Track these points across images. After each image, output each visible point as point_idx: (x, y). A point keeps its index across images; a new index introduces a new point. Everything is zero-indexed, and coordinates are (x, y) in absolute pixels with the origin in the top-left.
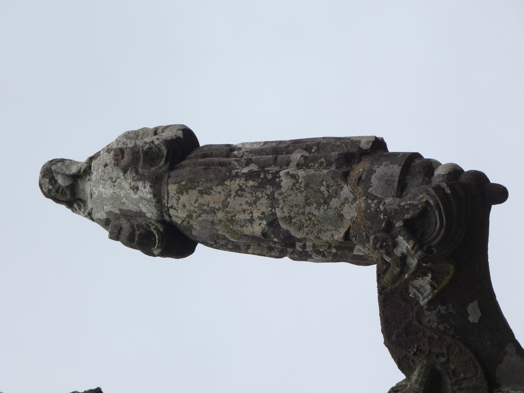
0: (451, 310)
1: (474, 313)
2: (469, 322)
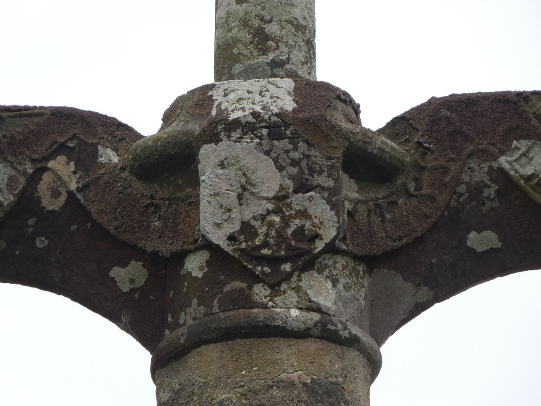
0: (488, 204)
1: (480, 240)
2: (469, 232)
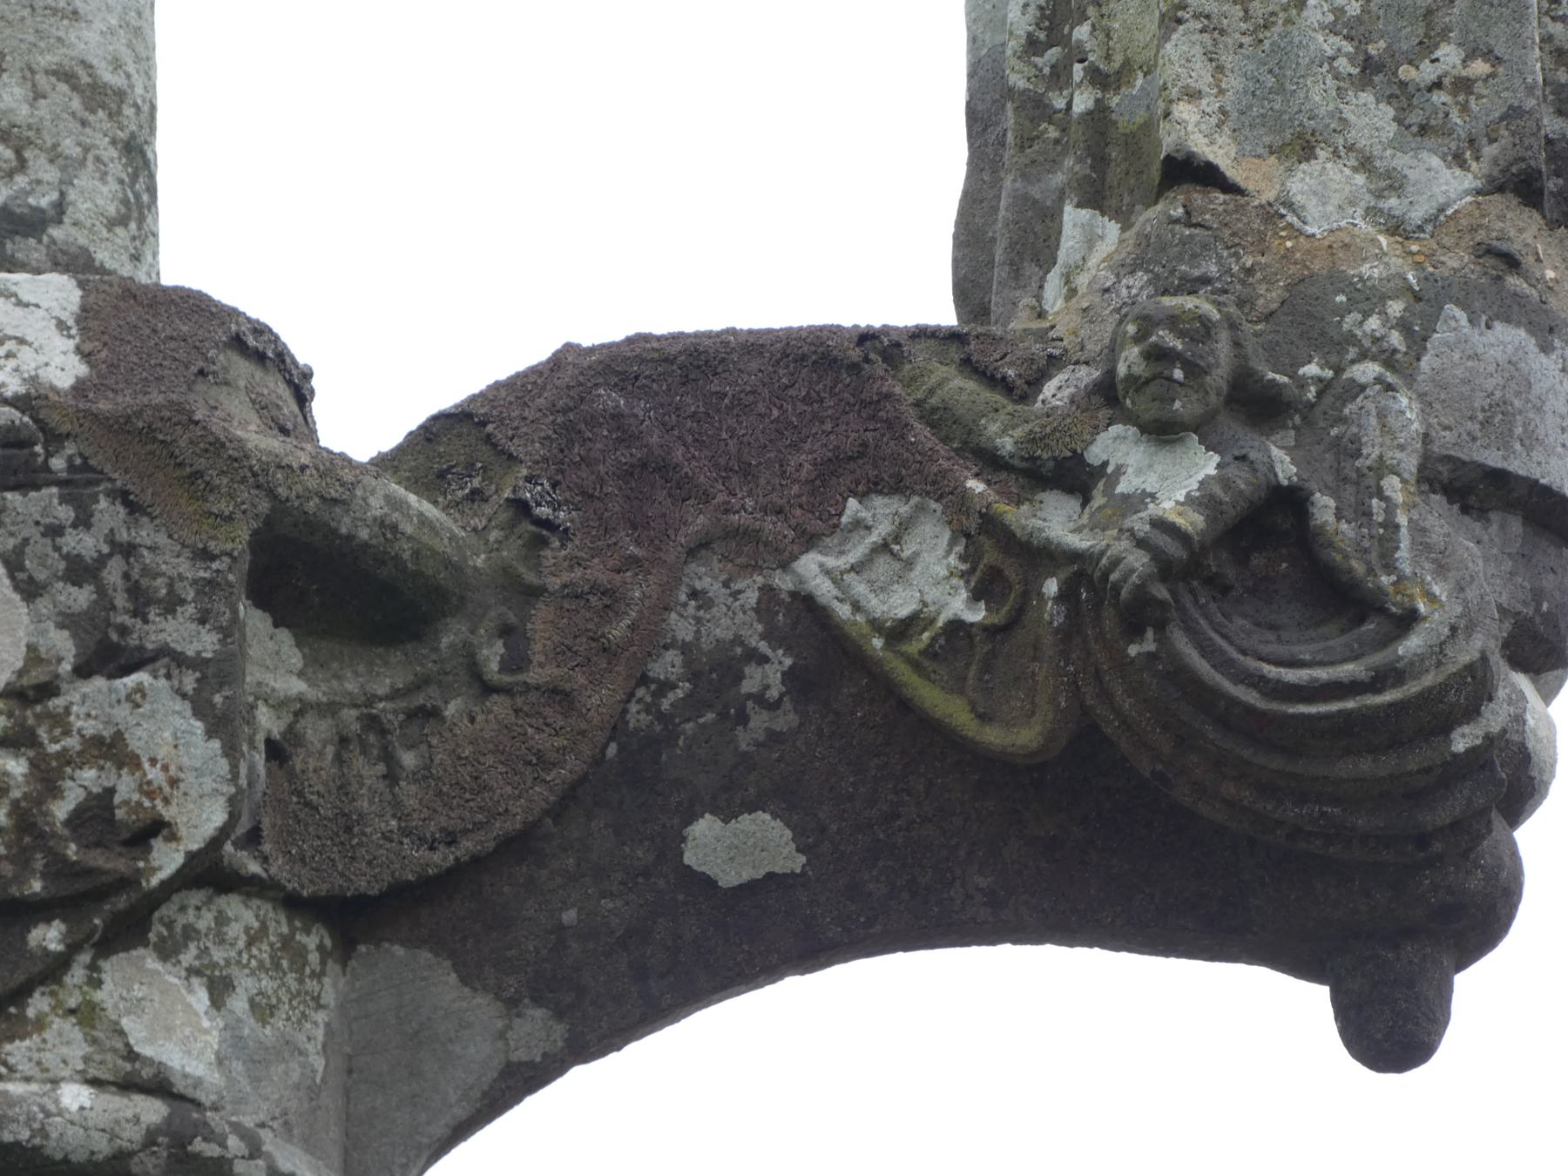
1: (733, 846)
